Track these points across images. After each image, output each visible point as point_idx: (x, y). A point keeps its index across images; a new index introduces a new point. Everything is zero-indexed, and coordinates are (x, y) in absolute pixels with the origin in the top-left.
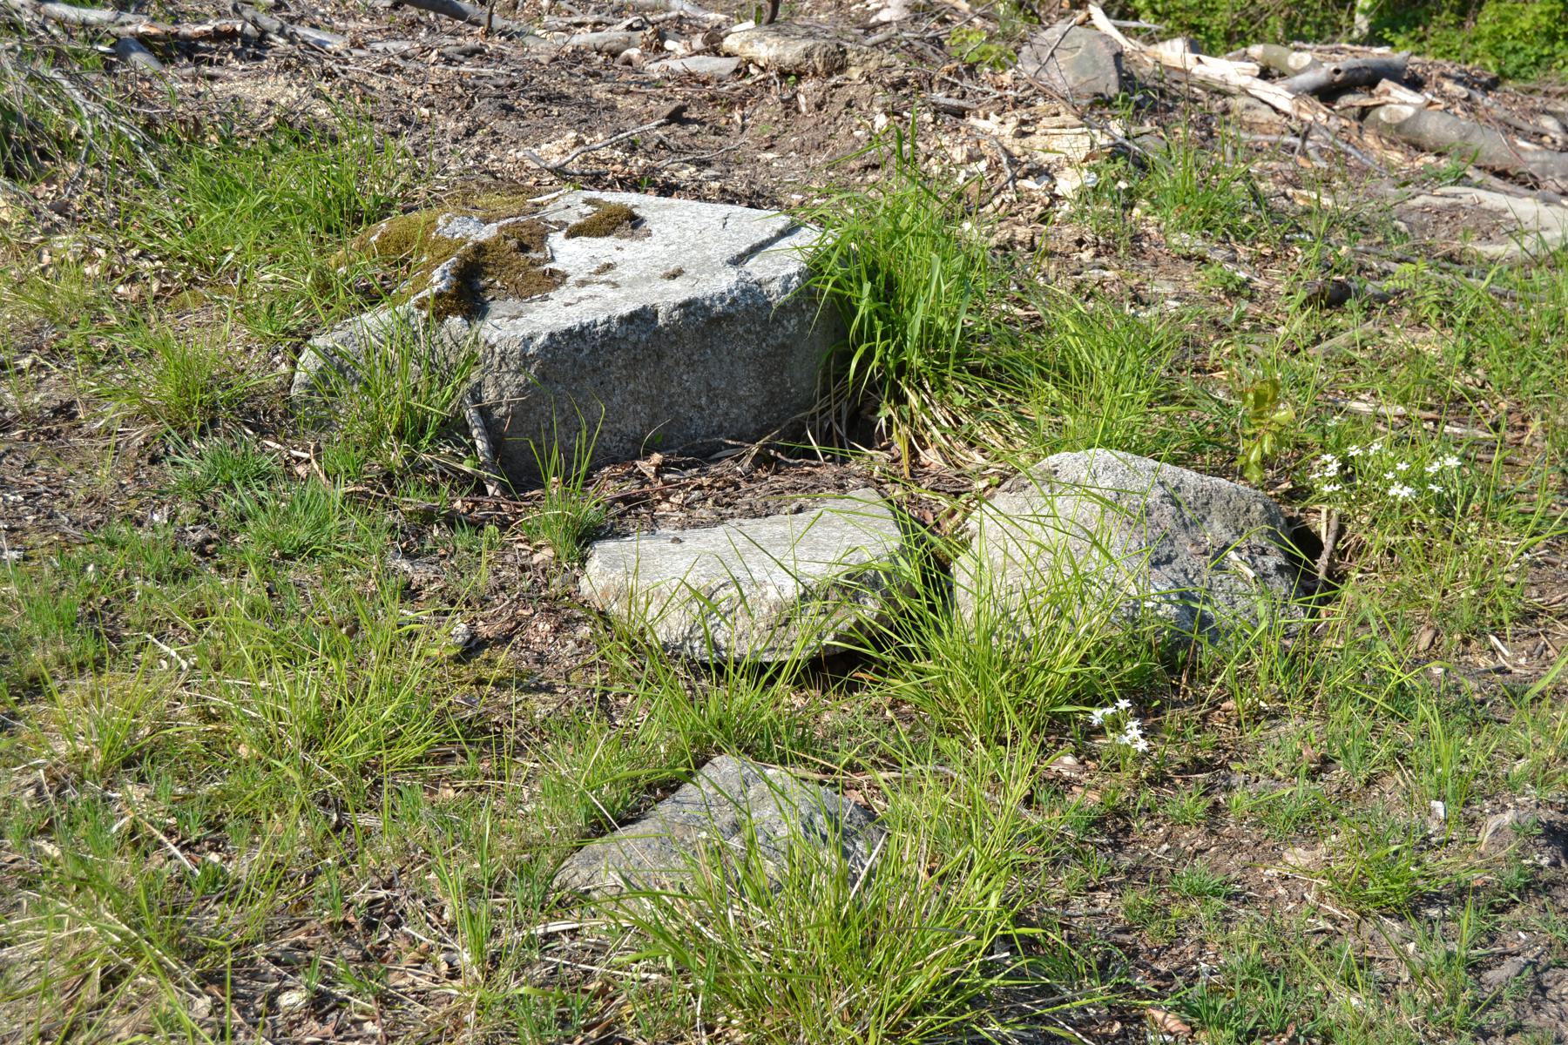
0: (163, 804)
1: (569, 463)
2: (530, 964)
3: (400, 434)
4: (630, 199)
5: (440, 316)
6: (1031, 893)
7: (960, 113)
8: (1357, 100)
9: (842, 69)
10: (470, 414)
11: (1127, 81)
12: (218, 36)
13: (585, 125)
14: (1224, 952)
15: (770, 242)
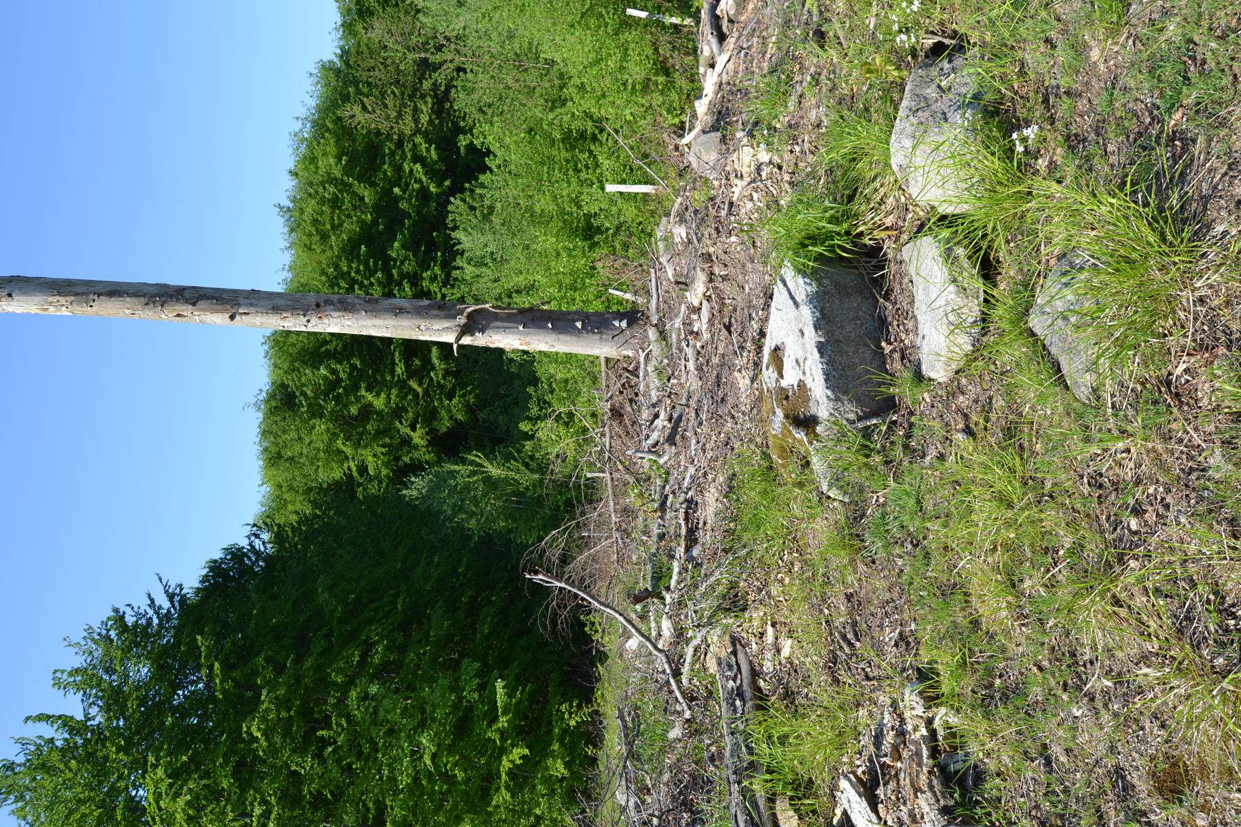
0: (1034, 572)
1: (884, 383)
2: (1126, 416)
3: (867, 456)
4: (766, 351)
5: (817, 435)
6: (1108, 181)
7: (731, 204)
8: (725, 25)
9: (710, 255)
10: (860, 425)
11: (714, 128)
12: (687, 519)
13: (731, 368)
14: (1143, 91)
15: (789, 290)
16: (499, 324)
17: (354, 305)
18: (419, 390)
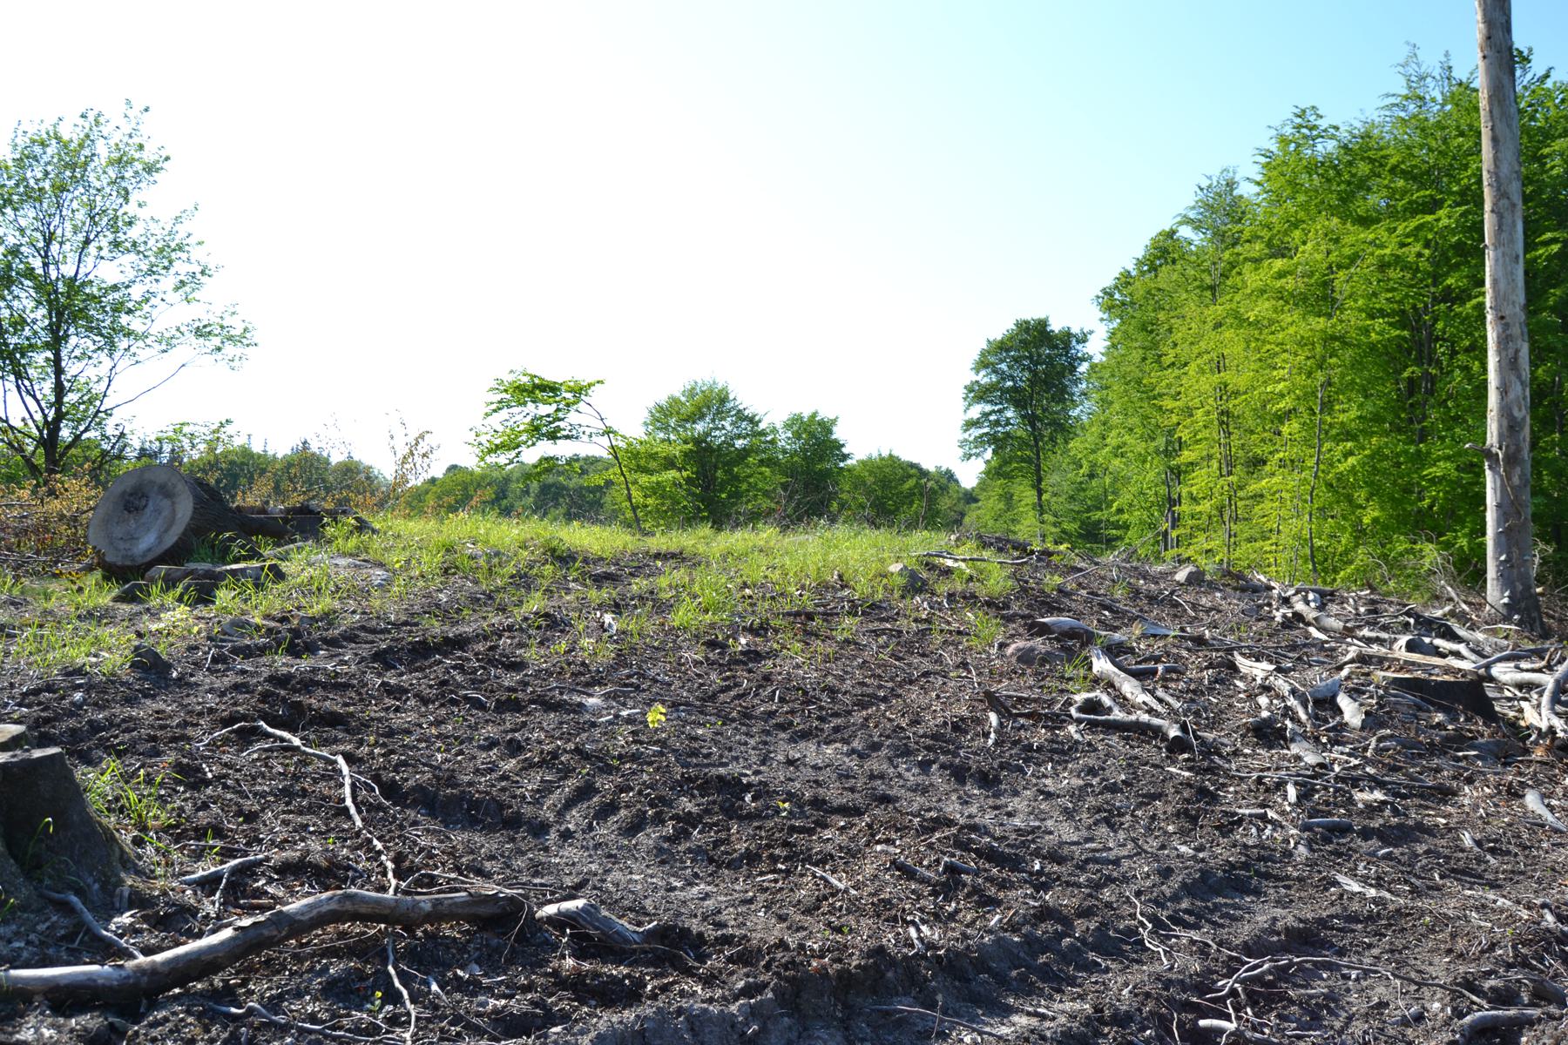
17: (1506, 349)
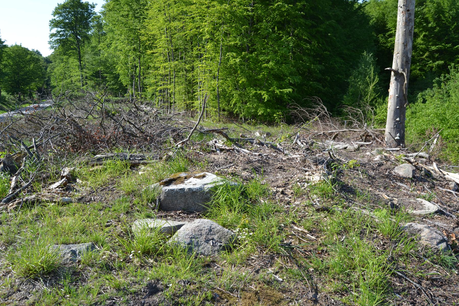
16: (399, 86)
17: (408, 25)
18: (424, 57)
